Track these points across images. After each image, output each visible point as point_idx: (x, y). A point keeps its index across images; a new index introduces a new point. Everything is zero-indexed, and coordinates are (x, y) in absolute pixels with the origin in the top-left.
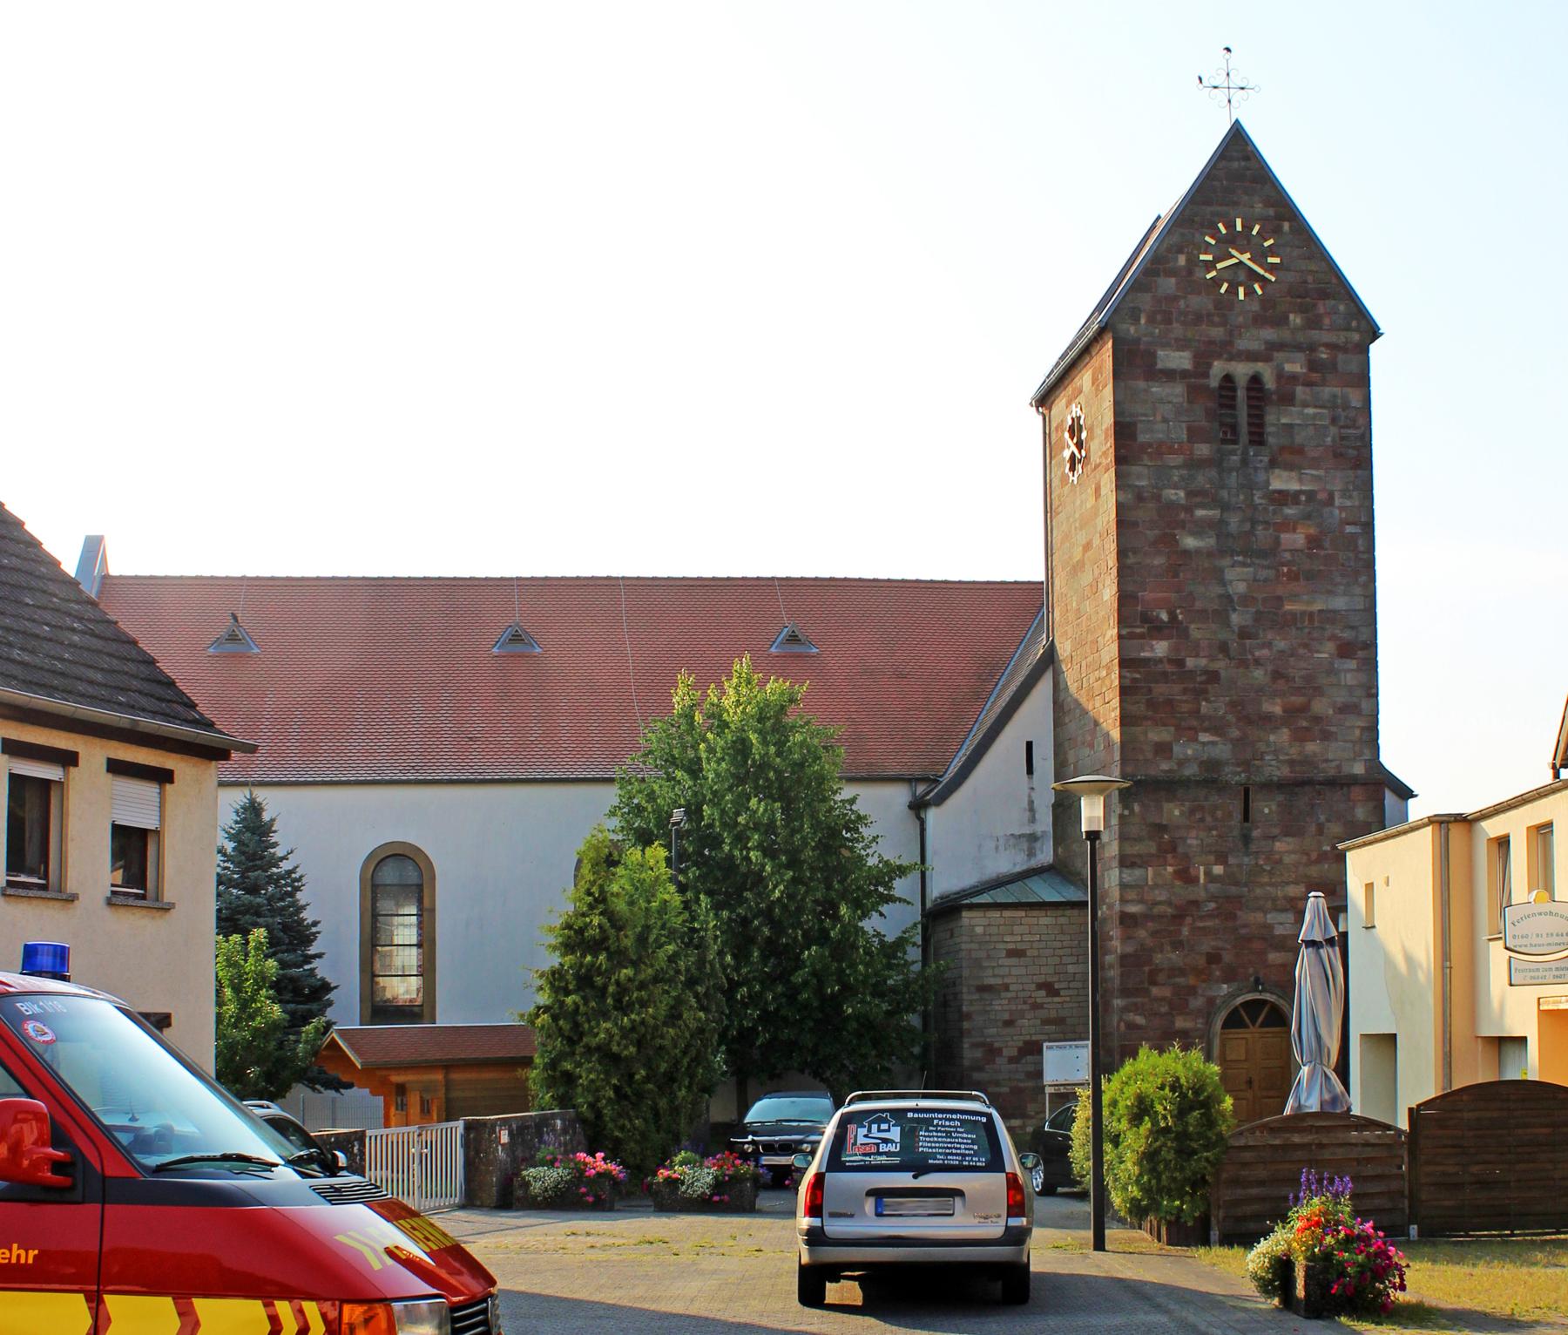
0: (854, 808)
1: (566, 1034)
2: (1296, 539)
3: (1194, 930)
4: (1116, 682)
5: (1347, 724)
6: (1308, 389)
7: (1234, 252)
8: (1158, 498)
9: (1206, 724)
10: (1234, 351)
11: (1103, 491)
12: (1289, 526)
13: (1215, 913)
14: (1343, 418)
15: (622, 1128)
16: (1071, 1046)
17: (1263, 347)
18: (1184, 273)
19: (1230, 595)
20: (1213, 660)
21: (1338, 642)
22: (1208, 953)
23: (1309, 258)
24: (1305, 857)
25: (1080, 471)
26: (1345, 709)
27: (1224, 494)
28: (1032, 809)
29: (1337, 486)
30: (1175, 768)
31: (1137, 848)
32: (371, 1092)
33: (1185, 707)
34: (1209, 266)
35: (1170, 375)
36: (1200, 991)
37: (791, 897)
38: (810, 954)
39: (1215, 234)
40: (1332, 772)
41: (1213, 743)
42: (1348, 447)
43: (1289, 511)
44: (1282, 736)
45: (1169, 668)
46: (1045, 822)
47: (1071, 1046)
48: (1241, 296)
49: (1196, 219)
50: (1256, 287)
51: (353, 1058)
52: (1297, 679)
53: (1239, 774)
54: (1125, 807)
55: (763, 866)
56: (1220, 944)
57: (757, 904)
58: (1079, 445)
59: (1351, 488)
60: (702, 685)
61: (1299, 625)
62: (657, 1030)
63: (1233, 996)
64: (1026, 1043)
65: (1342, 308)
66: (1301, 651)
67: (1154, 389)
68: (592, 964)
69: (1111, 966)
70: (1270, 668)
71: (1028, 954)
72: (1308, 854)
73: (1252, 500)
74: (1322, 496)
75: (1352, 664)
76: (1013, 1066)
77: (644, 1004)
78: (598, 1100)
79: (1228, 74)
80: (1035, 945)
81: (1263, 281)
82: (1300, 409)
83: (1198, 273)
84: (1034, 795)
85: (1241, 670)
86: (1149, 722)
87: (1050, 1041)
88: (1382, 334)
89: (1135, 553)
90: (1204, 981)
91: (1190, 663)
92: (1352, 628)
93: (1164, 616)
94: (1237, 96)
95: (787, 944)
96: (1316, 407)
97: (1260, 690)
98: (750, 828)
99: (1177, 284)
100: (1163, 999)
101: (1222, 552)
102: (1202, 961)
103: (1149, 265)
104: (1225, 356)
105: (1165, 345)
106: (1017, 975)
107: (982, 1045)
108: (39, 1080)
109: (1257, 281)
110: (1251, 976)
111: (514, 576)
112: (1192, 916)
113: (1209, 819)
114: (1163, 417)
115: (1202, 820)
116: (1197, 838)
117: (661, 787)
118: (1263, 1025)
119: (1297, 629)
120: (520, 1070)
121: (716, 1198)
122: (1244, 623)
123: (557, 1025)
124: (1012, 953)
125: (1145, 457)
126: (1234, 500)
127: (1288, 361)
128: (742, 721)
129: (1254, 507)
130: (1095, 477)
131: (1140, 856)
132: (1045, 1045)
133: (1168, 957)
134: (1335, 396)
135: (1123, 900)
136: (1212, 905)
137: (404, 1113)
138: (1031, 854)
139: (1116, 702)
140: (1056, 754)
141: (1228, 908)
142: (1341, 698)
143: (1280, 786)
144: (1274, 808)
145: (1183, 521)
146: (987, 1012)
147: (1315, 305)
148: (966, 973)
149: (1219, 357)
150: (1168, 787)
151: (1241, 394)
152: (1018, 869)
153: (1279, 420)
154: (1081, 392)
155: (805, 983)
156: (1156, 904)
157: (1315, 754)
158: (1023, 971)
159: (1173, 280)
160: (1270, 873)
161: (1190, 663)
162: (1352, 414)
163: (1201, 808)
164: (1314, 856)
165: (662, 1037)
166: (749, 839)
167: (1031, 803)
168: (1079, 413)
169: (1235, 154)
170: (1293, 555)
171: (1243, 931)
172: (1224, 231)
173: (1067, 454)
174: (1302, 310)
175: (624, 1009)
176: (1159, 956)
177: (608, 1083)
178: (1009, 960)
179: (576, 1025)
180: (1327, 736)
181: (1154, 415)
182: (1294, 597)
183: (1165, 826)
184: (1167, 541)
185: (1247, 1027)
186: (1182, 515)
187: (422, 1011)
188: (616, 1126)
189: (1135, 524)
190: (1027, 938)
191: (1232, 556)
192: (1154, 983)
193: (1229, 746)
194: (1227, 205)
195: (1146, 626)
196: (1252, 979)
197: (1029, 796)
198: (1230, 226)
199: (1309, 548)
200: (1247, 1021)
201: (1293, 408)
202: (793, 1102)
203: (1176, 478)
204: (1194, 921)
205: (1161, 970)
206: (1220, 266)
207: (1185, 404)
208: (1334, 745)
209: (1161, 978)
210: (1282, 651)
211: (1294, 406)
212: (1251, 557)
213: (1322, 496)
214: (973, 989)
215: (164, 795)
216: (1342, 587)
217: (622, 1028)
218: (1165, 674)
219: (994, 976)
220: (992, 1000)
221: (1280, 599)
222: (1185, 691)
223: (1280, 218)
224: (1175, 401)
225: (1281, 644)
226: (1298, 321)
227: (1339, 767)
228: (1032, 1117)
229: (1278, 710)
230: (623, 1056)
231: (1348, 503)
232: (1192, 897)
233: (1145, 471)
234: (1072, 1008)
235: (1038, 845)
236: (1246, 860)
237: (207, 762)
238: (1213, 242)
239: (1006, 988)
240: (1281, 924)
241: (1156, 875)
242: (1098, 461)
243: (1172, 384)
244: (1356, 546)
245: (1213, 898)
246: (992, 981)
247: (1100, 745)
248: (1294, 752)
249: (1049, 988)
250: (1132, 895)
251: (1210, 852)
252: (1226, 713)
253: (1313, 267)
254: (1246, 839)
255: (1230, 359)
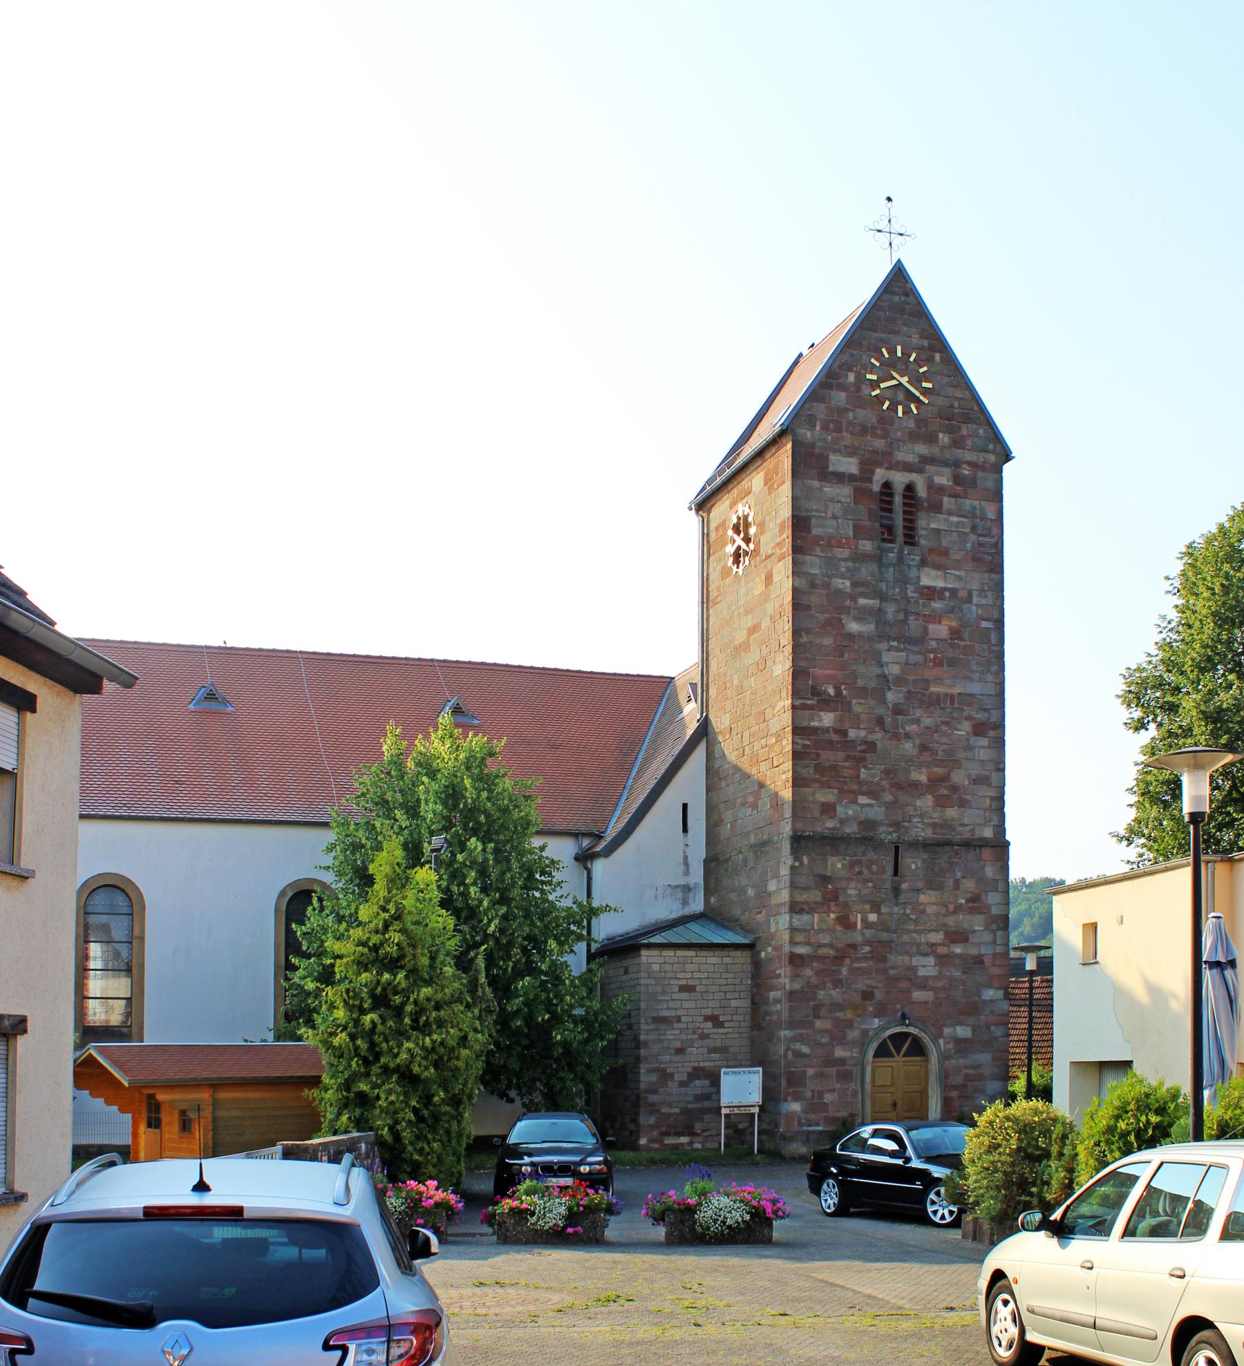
0: (544, 854)
1: (362, 1054)
2: (940, 630)
3: (851, 970)
4: (789, 747)
5: (980, 794)
6: (953, 500)
7: (895, 374)
8: (827, 585)
9: (864, 788)
10: (893, 462)
11: (776, 578)
12: (936, 618)
13: (869, 955)
14: (980, 528)
15: (421, 1152)
16: (744, 1072)
17: (917, 460)
18: (853, 389)
19: (885, 676)
20: (870, 732)
21: (974, 722)
22: (863, 991)
23: (955, 387)
24: (945, 909)
25: (747, 563)
26: (981, 780)
27: (883, 586)
28: (686, 863)
29: (975, 586)
30: (838, 826)
31: (805, 896)
32: (119, 1110)
33: (847, 773)
34: (874, 385)
35: (840, 478)
37: (502, 931)
38: (524, 984)
39: (880, 357)
40: (967, 836)
41: (870, 806)
42: (985, 553)
43: (937, 605)
44: (927, 802)
45: (835, 737)
46: (697, 876)
47: (744, 1072)
48: (900, 414)
49: (864, 342)
50: (913, 406)
51: (117, 1075)
52: (939, 752)
53: (891, 833)
54: (796, 859)
55: (481, 902)
56: (873, 983)
57: (472, 937)
58: (747, 540)
59: (986, 589)
60: (409, 736)
61: (942, 705)
62: (454, 1052)
63: (883, 1028)
64: (695, 1069)
65: (981, 432)
66: (944, 728)
67: (825, 489)
68: (389, 983)
69: (777, 1001)
70: (917, 742)
71: (697, 990)
72: (946, 907)
73: (906, 593)
74: (962, 594)
75: (984, 742)
76: (684, 1089)
77: (441, 1024)
78: (397, 1122)
79: (890, 221)
80: (704, 982)
81: (917, 401)
82: (946, 516)
83: (865, 390)
84: (688, 853)
85: (894, 742)
86: (817, 785)
87: (727, 1067)
88: (1014, 457)
89: (807, 633)
91: (852, 734)
92: (985, 710)
93: (831, 691)
94: (897, 240)
95: (498, 975)
96: (959, 516)
97: (910, 760)
98: (466, 865)
99: (847, 397)
100: (825, 1031)
101: (881, 637)
102: (857, 998)
103: (824, 379)
104: (886, 465)
105: (838, 451)
106: (688, 1009)
107: (657, 1070)
109: (913, 402)
110: (898, 1012)
111: (203, 645)
112: (851, 958)
113: (866, 872)
114: (833, 514)
115: (860, 873)
116: (855, 889)
117: (382, 825)
118: (905, 1055)
119: (941, 708)
120: (306, 1091)
121: (570, 1230)
122: (897, 702)
123: (354, 1044)
124: (684, 989)
125: (818, 549)
126: (890, 592)
127: (938, 474)
128: (454, 767)
129: (908, 600)
130: (766, 567)
131: (806, 903)
132: (723, 1070)
133: (829, 994)
134: (974, 508)
135: (792, 943)
136: (867, 949)
137: (158, 1131)
138: (685, 903)
139: (788, 765)
140: (708, 816)
141: (881, 950)
142: (975, 770)
143: (926, 845)
144: (919, 864)
145: (849, 608)
146: (662, 1041)
147: (959, 428)
148: (643, 1005)
149: (880, 465)
150: (833, 842)
151: (898, 500)
152: (674, 916)
153: (928, 525)
154: (750, 492)
155: (518, 1011)
156: (820, 946)
157: (953, 820)
158: (692, 1004)
159: (843, 394)
160: (916, 922)
161: (852, 734)
162: (989, 524)
163: (859, 862)
164: (951, 908)
165: (458, 1058)
166: (465, 877)
167: (686, 858)
168: (747, 510)
169: (897, 289)
170: (938, 643)
171: (892, 972)
172: (887, 356)
173: (730, 549)
174: (950, 430)
175: (425, 1029)
176: (822, 992)
177: (407, 1104)
178: (679, 994)
179: (373, 1045)
180: (963, 804)
181: (826, 513)
182: (939, 680)
183: (830, 877)
184: (834, 624)
185: (893, 1056)
186: (848, 603)
187: (131, 1031)
188: (415, 1149)
189: (808, 608)
190: (696, 975)
191: (888, 641)
192: (817, 1016)
193: (883, 809)
194: (889, 333)
195: (816, 698)
196: (899, 1014)
197: (684, 852)
198: (892, 352)
199: (951, 639)
200: (904, 1049)
201: (941, 516)
202: (553, 1124)
203: (843, 569)
204: (852, 962)
205: (823, 1005)
206: (883, 385)
207: (852, 505)
209: (823, 1012)
210: (928, 728)
211: (941, 513)
212: (903, 643)
213: (962, 594)
214: (649, 1020)
215: (24, 726)
216: (977, 674)
217: (423, 1048)
218: (831, 742)
219: (668, 1009)
220: (665, 1030)
221: (927, 682)
222: (847, 758)
223: (932, 349)
224: (843, 500)
225: (927, 721)
226: (946, 440)
227: (972, 831)
228: (698, 1135)
229: (923, 778)
230: (423, 1077)
231: (984, 602)
232: (850, 942)
233: (817, 560)
234: (734, 1038)
235: (691, 895)
236: (896, 909)
237: (71, 693)
238: (878, 364)
239: (678, 1019)
240: (924, 966)
241: (821, 920)
242: (770, 552)
243: (840, 486)
244: (989, 641)
245: (869, 943)
246: (666, 1013)
247: (765, 804)
248: (936, 816)
249: (715, 1020)
250: (800, 938)
251: (867, 902)
252: (881, 779)
253: (959, 394)
254: (896, 891)
255: (890, 468)
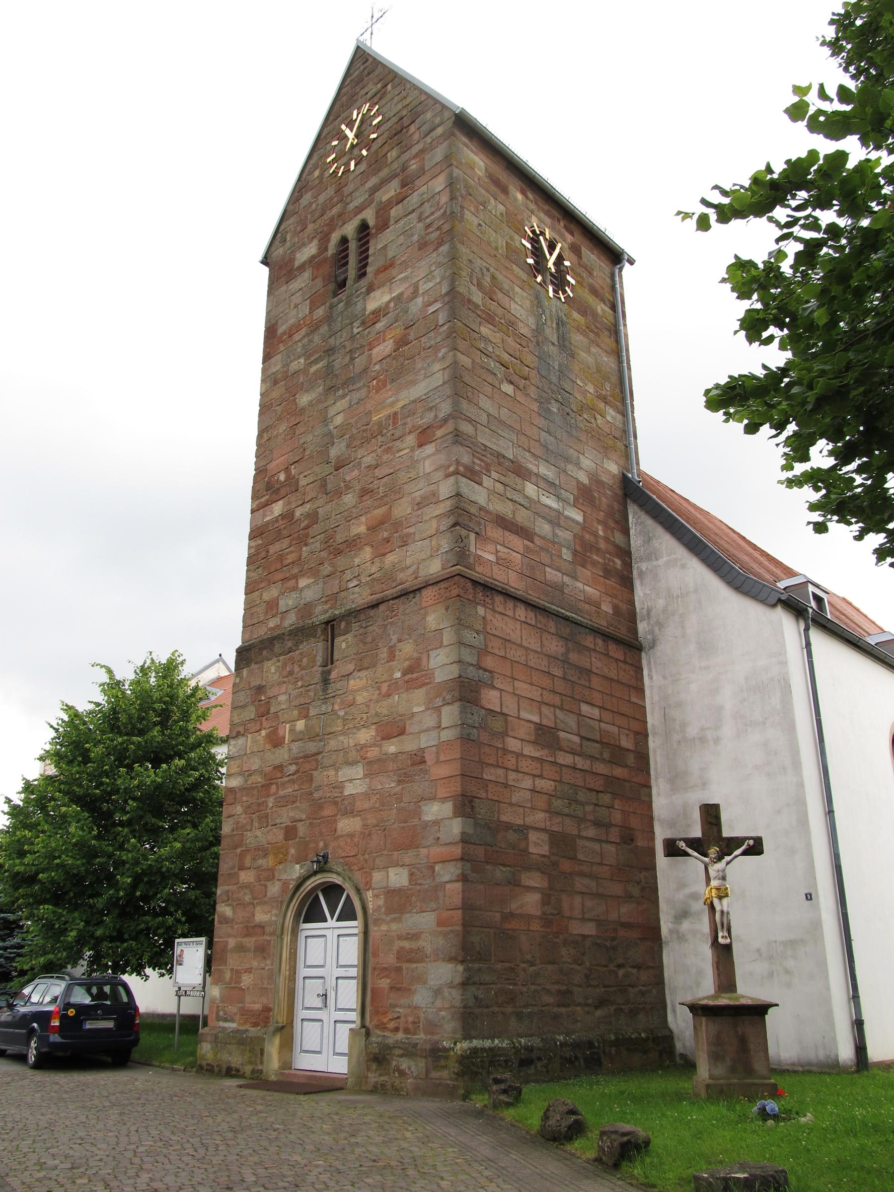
113: (296, 669)
208: (411, 548)
227: (417, 571)
229: (362, 529)
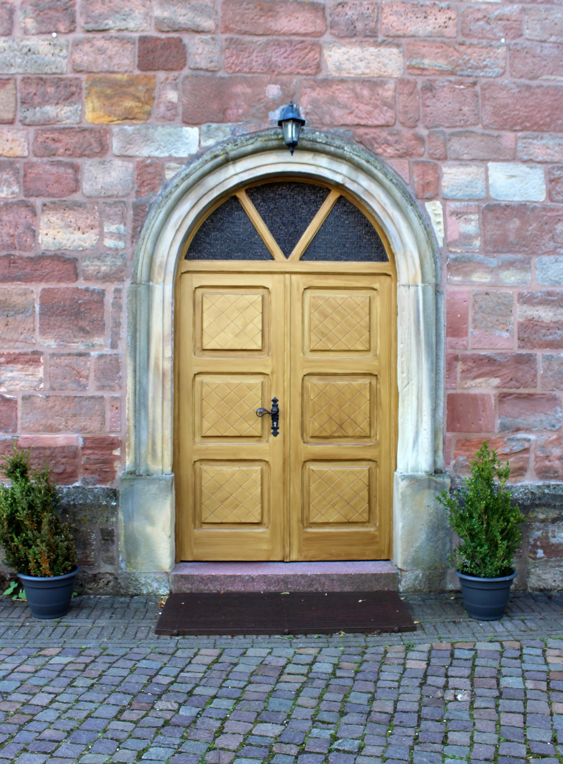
22: (143, 40)
36: (116, 145)
90: (128, 117)
108: (370, 313)
118: (306, 256)
